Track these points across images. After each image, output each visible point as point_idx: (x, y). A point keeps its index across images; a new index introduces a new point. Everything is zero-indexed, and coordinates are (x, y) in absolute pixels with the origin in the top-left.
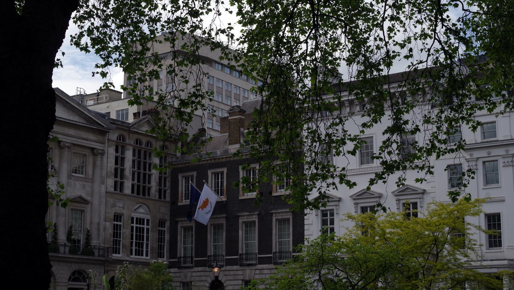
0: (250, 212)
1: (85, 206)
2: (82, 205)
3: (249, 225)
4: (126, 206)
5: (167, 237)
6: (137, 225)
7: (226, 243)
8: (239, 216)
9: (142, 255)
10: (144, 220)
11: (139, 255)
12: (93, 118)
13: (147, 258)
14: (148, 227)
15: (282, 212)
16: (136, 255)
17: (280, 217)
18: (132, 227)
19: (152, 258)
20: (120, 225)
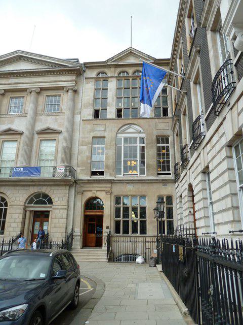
4: (107, 129)
12: (57, 62)
18: (118, 150)
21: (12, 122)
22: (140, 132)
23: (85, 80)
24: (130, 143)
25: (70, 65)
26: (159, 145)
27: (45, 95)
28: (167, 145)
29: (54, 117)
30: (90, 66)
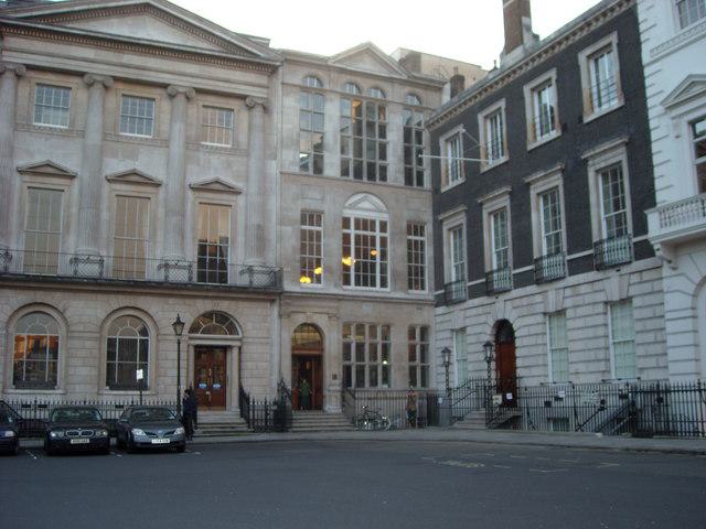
0: (545, 169)
1: (233, 198)
2: (225, 196)
3: (549, 195)
4: (328, 198)
5: (429, 252)
6: (358, 232)
7: (514, 245)
8: (529, 184)
9: (373, 285)
10: (373, 222)
11: (365, 284)
12: (233, 41)
13: (384, 289)
14: (383, 235)
15: (605, 152)
16: (357, 284)
17: (603, 165)
18: (346, 238)
19: (394, 290)
20: (318, 233)
21: (134, 156)
22: (381, 211)
23: (280, 87)
24: (365, 229)
25: (262, 55)
26: (304, 227)
27: (201, 104)
28: (422, 238)
29: (223, 158)
30: (292, 59)
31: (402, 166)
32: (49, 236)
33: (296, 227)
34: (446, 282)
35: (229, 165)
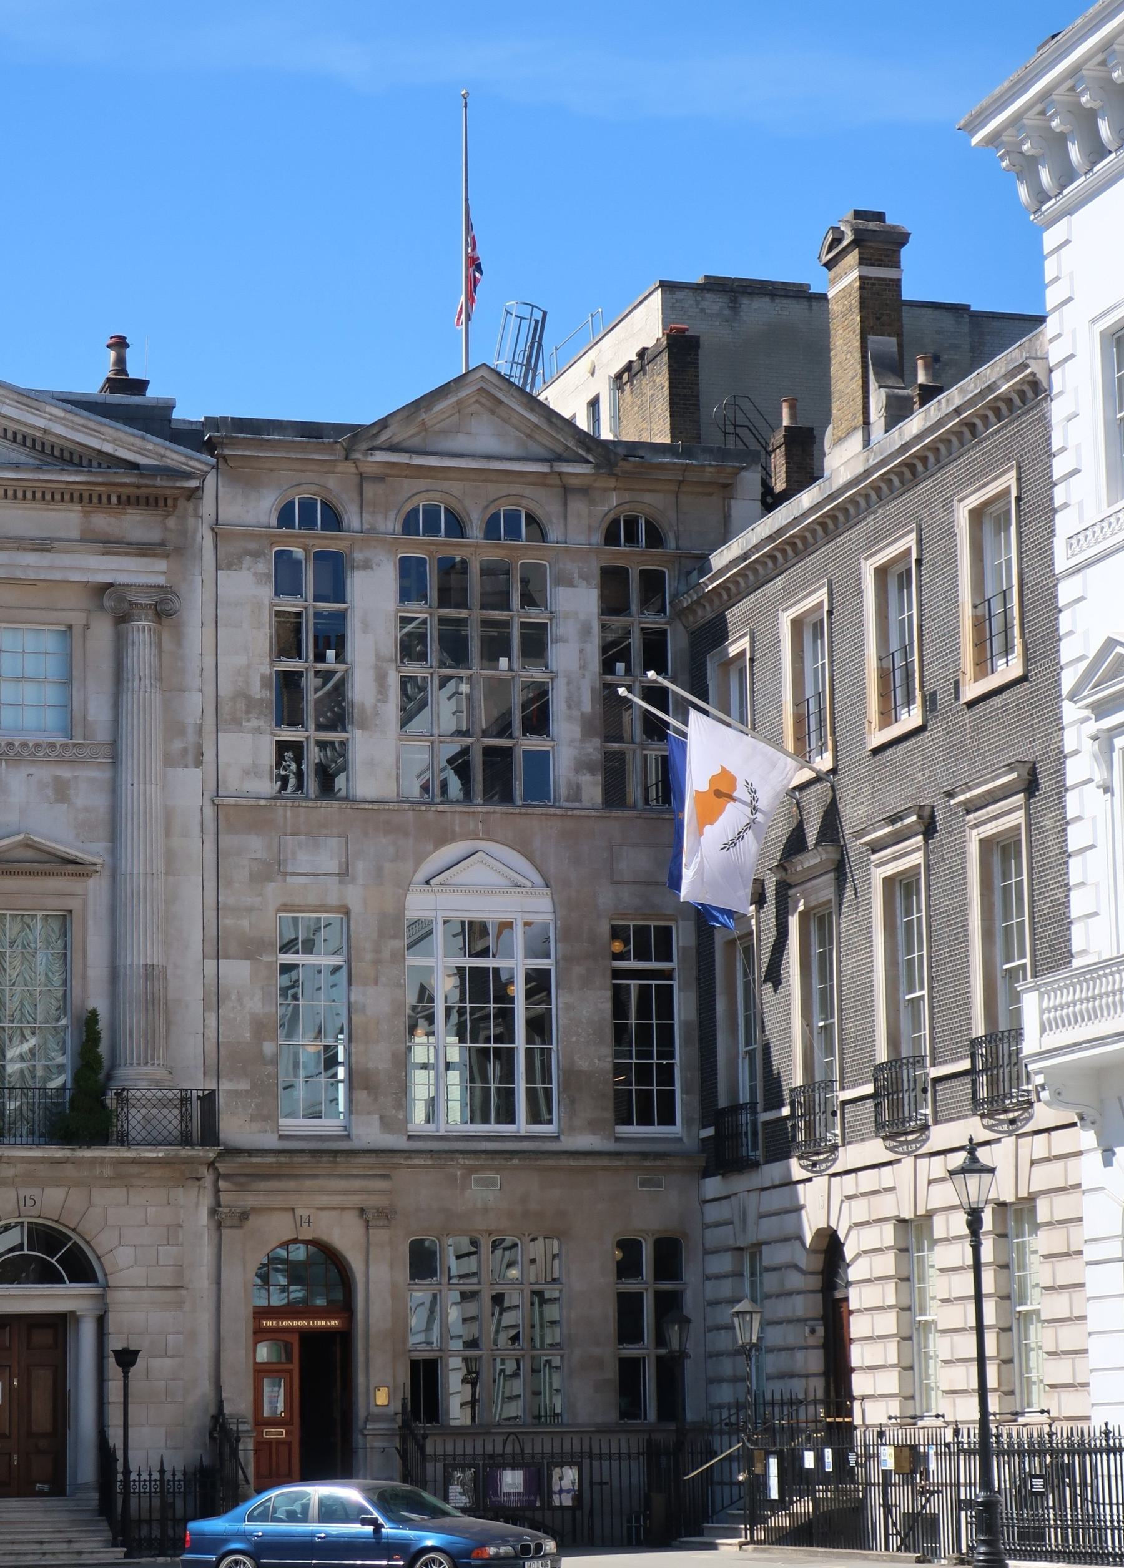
4: (360, 867)
29: (45, 773)
31: (594, 748)
32: (7, 1091)
33: (266, 958)
34: (723, 1102)
35: (61, 792)
